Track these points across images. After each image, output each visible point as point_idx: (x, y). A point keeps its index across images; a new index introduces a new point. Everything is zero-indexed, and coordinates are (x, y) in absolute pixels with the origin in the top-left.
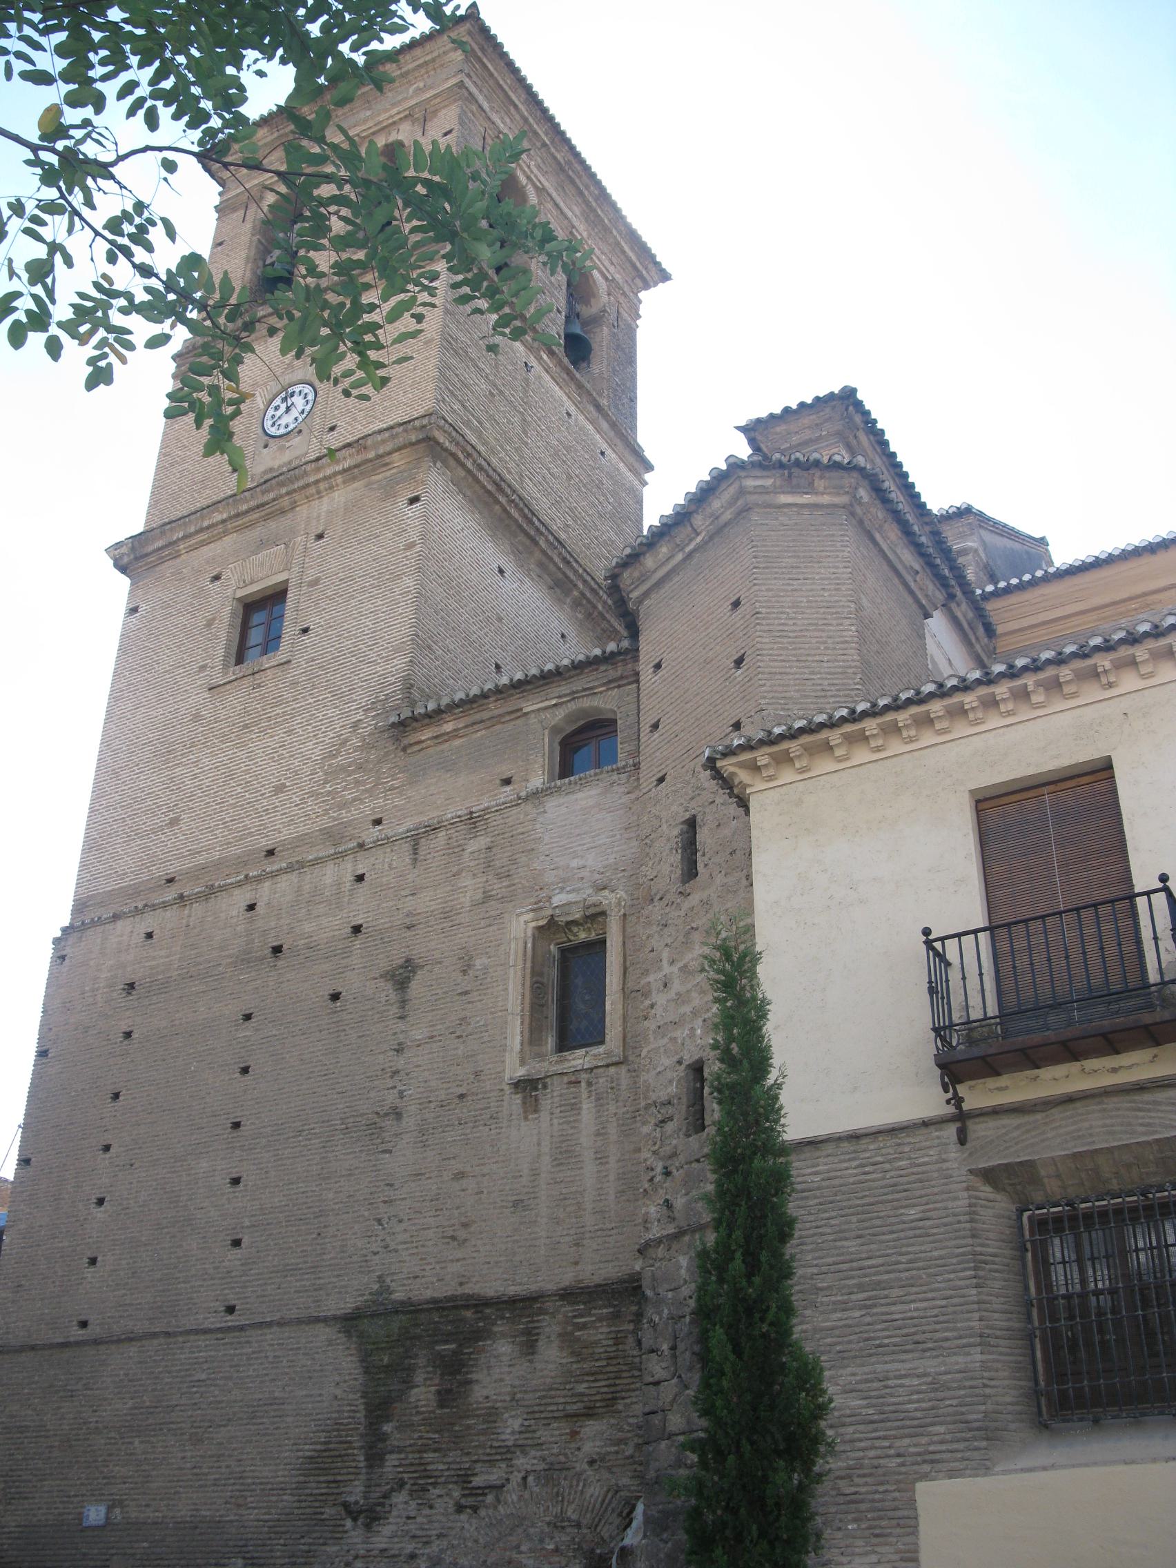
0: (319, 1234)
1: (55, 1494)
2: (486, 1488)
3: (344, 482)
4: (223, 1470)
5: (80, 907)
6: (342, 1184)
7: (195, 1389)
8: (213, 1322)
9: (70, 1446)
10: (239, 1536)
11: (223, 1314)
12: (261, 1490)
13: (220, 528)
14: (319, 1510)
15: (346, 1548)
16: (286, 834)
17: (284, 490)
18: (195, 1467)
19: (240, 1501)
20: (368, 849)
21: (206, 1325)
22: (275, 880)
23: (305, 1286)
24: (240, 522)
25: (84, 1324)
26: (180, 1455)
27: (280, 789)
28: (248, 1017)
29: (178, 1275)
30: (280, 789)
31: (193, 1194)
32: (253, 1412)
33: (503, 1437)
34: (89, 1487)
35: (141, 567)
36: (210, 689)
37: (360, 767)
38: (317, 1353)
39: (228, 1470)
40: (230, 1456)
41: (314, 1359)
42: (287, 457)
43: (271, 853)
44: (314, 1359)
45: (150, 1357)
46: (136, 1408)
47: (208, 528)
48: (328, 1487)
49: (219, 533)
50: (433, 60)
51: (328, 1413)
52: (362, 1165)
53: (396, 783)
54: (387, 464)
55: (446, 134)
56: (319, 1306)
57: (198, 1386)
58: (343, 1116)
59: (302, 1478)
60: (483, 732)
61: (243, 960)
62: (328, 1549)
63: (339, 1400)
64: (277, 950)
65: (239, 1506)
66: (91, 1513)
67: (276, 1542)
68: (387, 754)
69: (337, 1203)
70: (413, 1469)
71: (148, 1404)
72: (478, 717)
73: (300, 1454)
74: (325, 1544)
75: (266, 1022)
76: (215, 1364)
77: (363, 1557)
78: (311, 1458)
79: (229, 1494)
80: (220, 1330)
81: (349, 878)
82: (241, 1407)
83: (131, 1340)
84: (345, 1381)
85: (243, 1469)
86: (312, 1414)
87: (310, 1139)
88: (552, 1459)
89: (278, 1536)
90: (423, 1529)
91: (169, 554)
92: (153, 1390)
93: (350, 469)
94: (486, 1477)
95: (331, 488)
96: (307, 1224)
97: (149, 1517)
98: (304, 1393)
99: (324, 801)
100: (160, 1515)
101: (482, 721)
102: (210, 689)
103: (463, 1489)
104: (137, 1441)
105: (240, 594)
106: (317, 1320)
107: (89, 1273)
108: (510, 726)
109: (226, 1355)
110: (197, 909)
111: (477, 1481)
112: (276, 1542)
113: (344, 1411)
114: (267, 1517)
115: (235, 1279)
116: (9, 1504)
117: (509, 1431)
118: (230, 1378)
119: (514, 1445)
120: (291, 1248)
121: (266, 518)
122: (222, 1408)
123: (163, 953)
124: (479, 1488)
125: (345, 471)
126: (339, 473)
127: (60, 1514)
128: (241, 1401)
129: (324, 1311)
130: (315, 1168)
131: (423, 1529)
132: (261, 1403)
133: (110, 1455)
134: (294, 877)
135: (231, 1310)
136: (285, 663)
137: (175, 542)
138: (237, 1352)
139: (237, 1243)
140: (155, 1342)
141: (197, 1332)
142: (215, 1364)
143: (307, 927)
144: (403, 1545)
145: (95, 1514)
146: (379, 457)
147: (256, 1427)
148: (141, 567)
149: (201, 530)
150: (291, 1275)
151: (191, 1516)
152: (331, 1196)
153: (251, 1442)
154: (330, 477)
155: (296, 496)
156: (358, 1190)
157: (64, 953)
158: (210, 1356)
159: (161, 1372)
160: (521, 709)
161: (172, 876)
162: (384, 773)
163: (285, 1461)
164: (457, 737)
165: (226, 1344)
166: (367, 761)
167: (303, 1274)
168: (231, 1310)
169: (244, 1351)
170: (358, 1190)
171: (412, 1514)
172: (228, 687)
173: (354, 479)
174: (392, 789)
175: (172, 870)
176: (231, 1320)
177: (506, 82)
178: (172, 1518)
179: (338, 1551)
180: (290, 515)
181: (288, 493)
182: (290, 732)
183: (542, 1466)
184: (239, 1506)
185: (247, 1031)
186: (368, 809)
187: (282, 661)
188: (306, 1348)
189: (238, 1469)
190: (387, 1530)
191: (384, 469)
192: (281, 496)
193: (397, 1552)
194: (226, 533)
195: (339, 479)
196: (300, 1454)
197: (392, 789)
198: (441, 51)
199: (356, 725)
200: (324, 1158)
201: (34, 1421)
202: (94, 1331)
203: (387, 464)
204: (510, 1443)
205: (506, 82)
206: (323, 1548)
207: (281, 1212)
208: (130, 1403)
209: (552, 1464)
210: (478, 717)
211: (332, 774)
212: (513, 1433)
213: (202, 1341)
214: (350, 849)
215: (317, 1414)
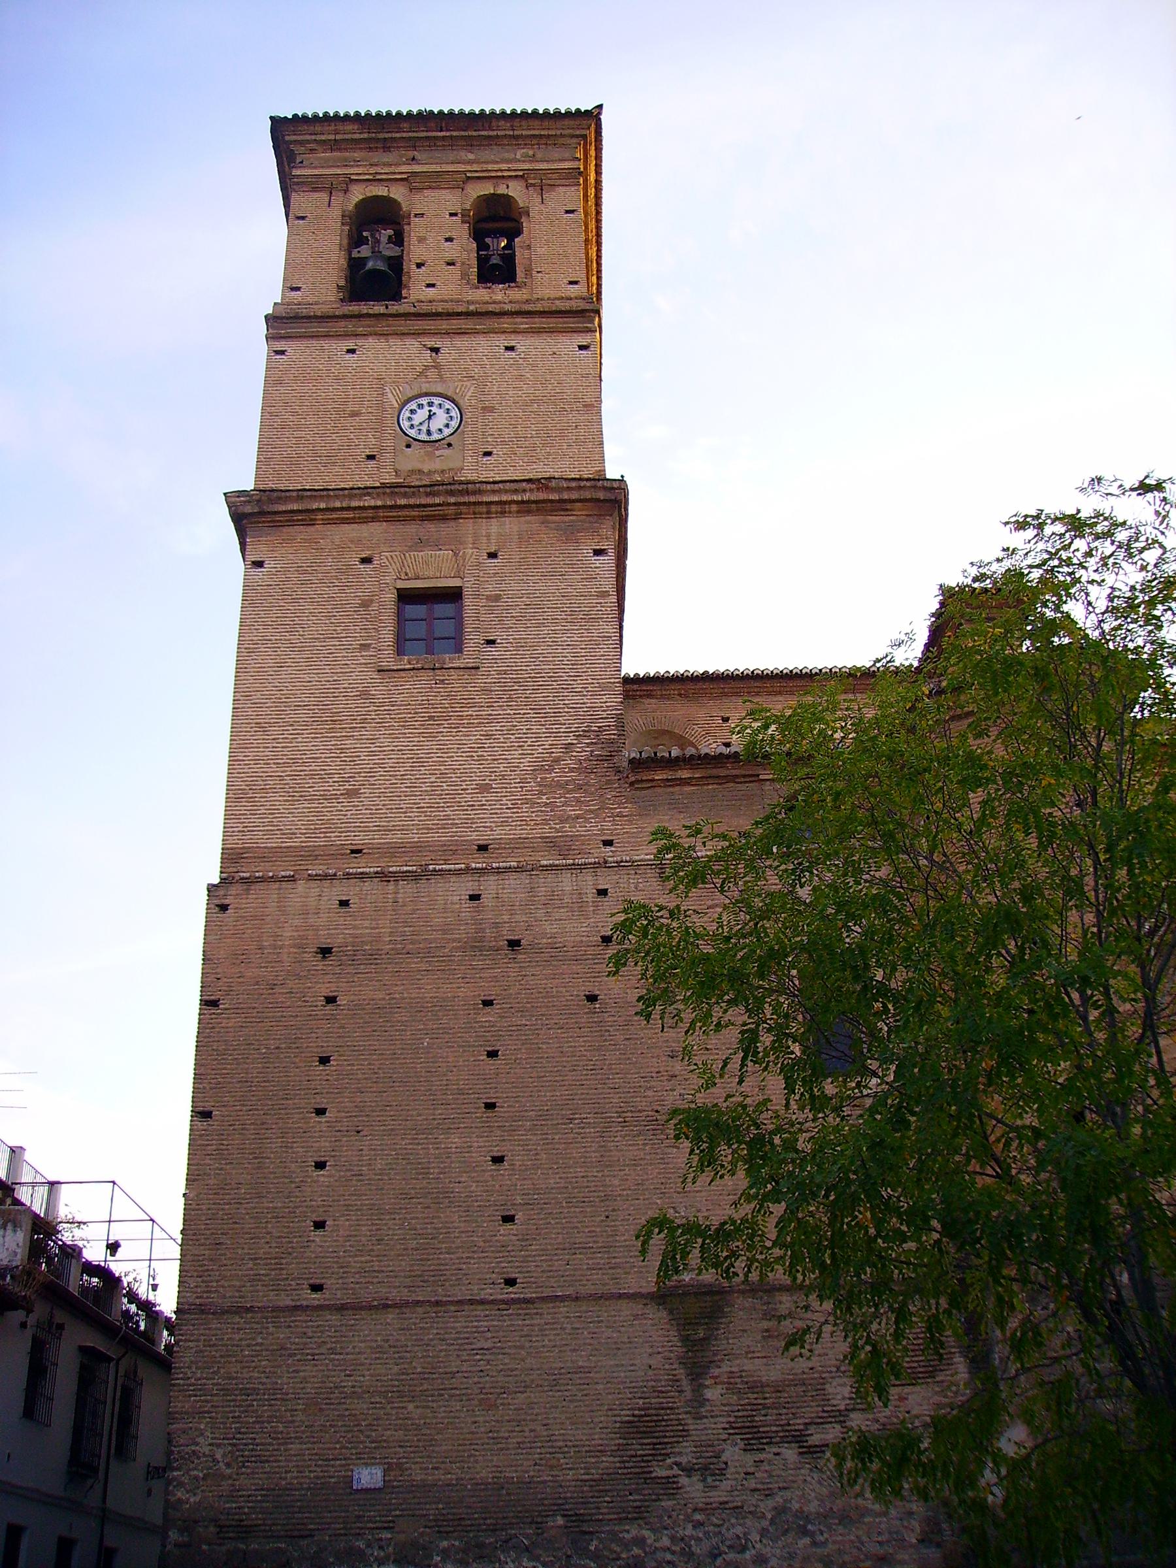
0: (607, 1217)
1: (307, 1458)
2: (823, 1446)
3: (518, 512)
4: (527, 1434)
5: (231, 857)
6: (627, 1172)
7: (478, 1357)
8: (487, 1293)
9: (321, 1410)
10: (557, 1495)
11: (503, 1286)
12: (575, 1452)
13: (370, 513)
14: (646, 1470)
15: (682, 1502)
16: (498, 833)
17: (452, 500)
18: (491, 1431)
19: (554, 1462)
20: (609, 867)
21: (483, 1295)
22: (502, 876)
23: (599, 1264)
24: (395, 514)
25: (317, 1288)
26: (469, 1420)
27: (484, 788)
28: (487, 1003)
29: (440, 1246)
30: (484, 788)
31: (445, 1167)
32: (554, 1380)
33: (835, 1402)
34: (354, 1451)
35: (264, 522)
36: (379, 671)
37: (579, 788)
38: (623, 1326)
39: (532, 1434)
40: (534, 1421)
41: (619, 1331)
42: (437, 465)
43: (483, 848)
44: (619, 1331)
45: (415, 1324)
46: (403, 1374)
47: (355, 508)
48: (654, 1449)
49: (366, 518)
50: (549, 136)
51: (643, 1381)
52: (648, 1157)
53: (625, 811)
54: (567, 510)
55: (567, 212)
56: (617, 1283)
57: (482, 1354)
58: (620, 1110)
59: (621, 1441)
60: (715, 786)
61: (472, 947)
62: (663, 1504)
63: (654, 1369)
64: (514, 944)
65: (552, 1467)
66: (362, 1477)
67: (602, 1499)
68: (608, 782)
69: (624, 1190)
70: (744, 1431)
71: (419, 1370)
72: (715, 772)
73: (618, 1419)
74: (659, 1500)
75: (512, 1010)
76: (501, 1334)
77: (702, 1510)
78: (629, 1422)
79: (537, 1456)
80: (503, 1302)
81: (591, 892)
82: (539, 1375)
83: (386, 1306)
84: (659, 1353)
85: (551, 1432)
86: (625, 1382)
87: (583, 1128)
88: (882, 1420)
89: (604, 1494)
90: (764, 1483)
91: (302, 520)
92: (423, 1357)
93: (528, 502)
94: (823, 1436)
95: (503, 513)
96: (592, 1206)
97: (440, 1480)
98: (612, 1363)
99: (542, 811)
100: (454, 1477)
101: (718, 777)
102: (379, 671)
103: (800, 1447)
104: (411, 1406)
105: (401, 585)
106: (620, 1296)
107: (317, 1236)
108: (743, 787)
109: (512, 1325)
110: (406, 890)
111: (815, 1439)
112: (602, 1499)
113: (661, 1380)
114: (587, 1477)
115: (512, 1254)
116: (244, 1466)
117: (839, 1397)
118: (522, 1347)
119: (846, 1410)
120: (577, 1227)
121: (423, 519)
122: (516, 1376)
123: (367, 923)
124: (816, 1446)
125: (523, 502)
126: (517, 502)
127: (317, 1477)
128: (538, 1369)
129: (625, 1289)
130: (593, 1155)
131: (764, 1483)
132: (563, 1371)
133: (377, 1419)
134: (524, 878)
135: (511, 1282)
136: (473, 668)
137: (313, 511)
138: (527, 1322)
139: (508, 1219)
140: (420, 1310)
141: (471, 1302)
142: (501, 1334)
143: (549, 929)
144: (745, 1497)
145: (369, 1476)
146: (561, 501)
147: (560, 1393)
148: (264, 522)
149: (349, 509)
150: (580, 1253)
151: (493, 1478)
152: (616, 1182)
153: (557, 1407)
154: (505, 503)
155: (464, 509)
156: (647, 1180)
157: (226, 902)
158: (494, 1326)
159: (432, 1340)
160: (758, 775)
161: (360, 847)
162: (609, 799)
163: (601, 1425)
164: (689, 784)
165: (511, 1314)
166: (586, 784)
167: (594, 1253)
168: (511, 1282)
169: (535, 1322)
170: (647, 1180)
171: (752, 1470)
172: (402, 674)
173: (529, 512)
174: (620, 815)
175: (359, 840)
176: (513, 1292)
177: (504, 130)
178: (471, 1479)
179: (675, 1505)
180: (452, 523)
181: (455, 504)
182: (488, 736)
183: (877, 1426)
184: (552, 1467)
185: (488, 1016)
186: (594, 828)
187: (470, 665)
188: (608, 1321)
189: (545, 1433)
190: (726, 1485)
191: (562, 513)
192: (449, 504)
193: (739, 1504)
194: (374, 519)
195: (514, 508)
196: (618, 1419)
197: (620, 815)
198: (558, 132)
199: (568, 747)
200: (602, 1147)
201: (263, 1384)
202: (334, 1293)
203: (567, 510)
204: (842, 1408)
205: (504, 130)
206: (657, 1503)
207: (560, 1193)
208: (396, 1369)
209: (884, 1425)
210: (715, 772)
211: (546, 787)
212: (844, 1398)
213: (480, 1311)
214: (591, 864)
215: (631, 1382)
